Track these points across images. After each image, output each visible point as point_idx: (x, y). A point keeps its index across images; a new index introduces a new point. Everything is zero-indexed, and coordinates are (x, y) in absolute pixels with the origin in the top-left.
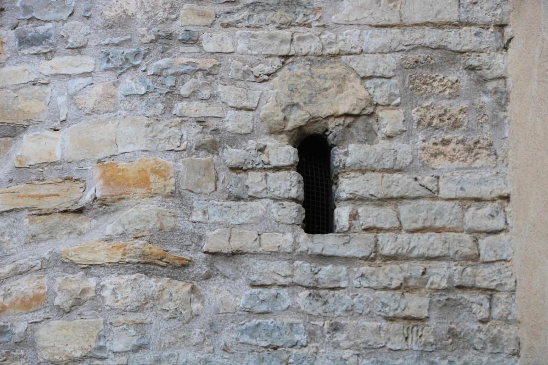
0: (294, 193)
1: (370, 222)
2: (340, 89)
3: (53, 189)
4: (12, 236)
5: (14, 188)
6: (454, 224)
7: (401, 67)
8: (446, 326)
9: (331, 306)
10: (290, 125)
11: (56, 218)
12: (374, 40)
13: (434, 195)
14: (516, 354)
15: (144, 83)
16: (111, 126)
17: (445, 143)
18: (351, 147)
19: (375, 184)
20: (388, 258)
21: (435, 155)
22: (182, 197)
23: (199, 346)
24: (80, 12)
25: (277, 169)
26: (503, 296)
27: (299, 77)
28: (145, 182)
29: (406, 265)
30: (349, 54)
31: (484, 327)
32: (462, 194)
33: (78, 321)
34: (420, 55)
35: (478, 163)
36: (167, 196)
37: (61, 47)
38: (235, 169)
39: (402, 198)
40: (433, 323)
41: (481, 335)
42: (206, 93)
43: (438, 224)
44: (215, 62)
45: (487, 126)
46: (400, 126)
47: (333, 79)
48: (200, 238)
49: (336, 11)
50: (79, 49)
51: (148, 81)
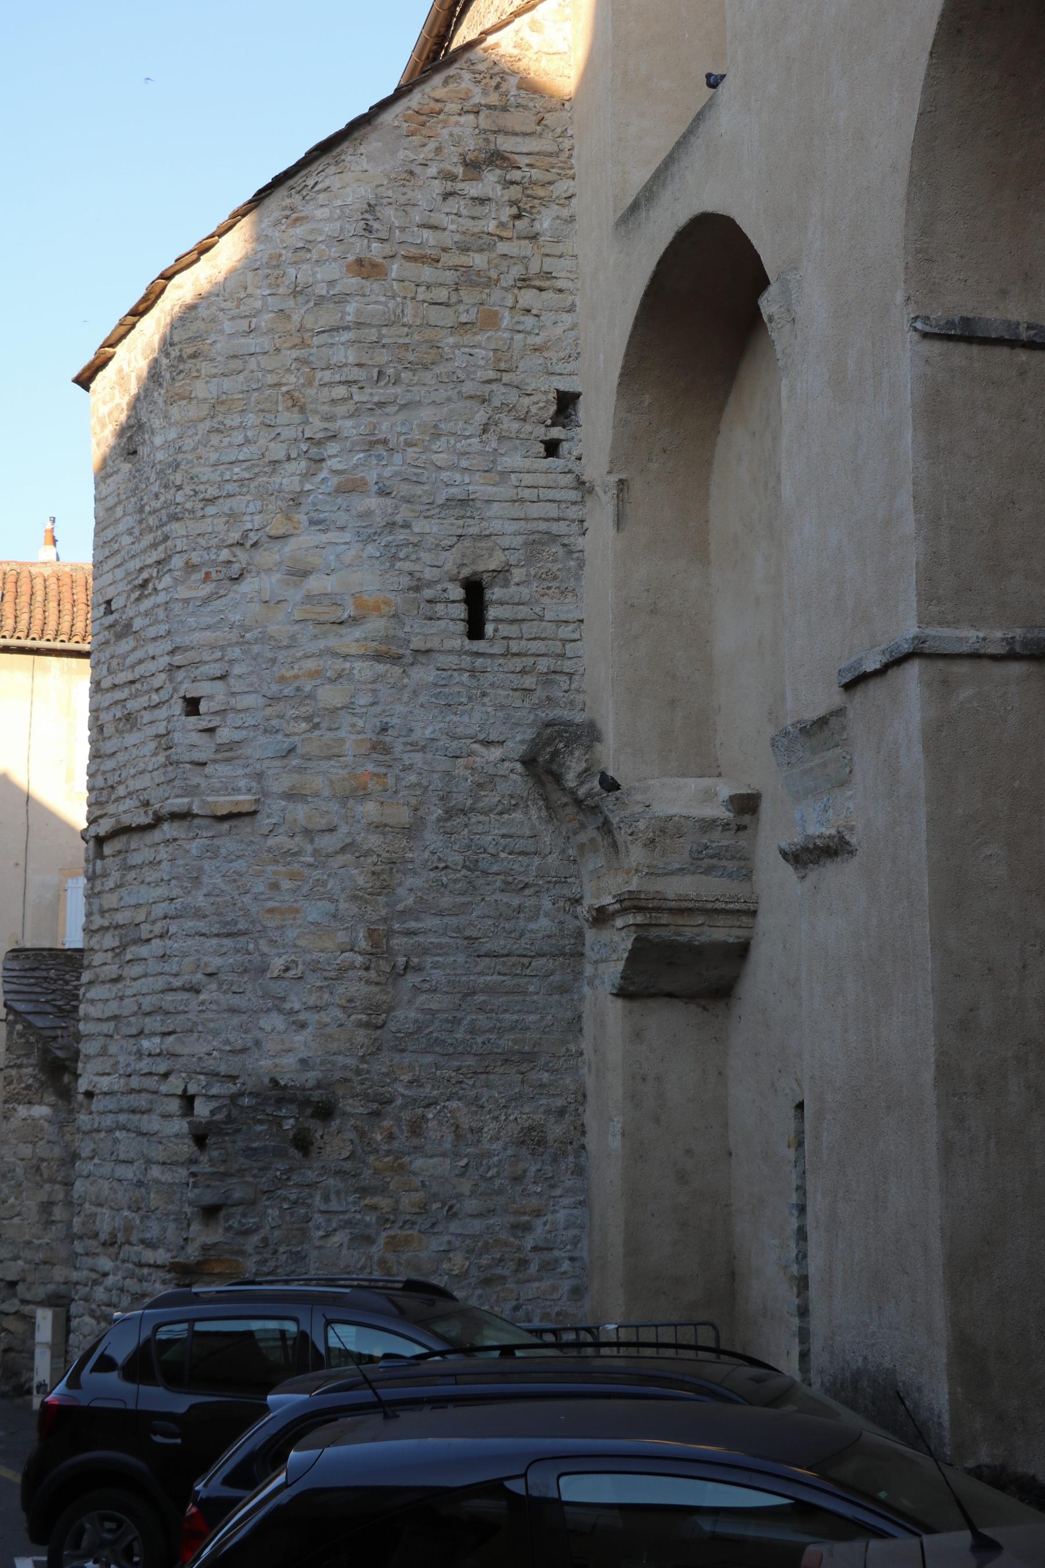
0: (462, 616)
1: (505, 634)
2: (490, 555)
3: (326, 609)
5: (304, 607)
6: (552, 636)
7: (525, 544)
8: (546, 694)
10: (461, 576)
11: (328, 626)
13: (541, 619)
14: (583, 710)
17: (549, 588)
18: (496, 590)
19: (518, 738)
20: (514, 655)
21: (543, 596)
23: (407, 704)
24: (344, 506)
25: (453, 602)
26: (577, 677)
28: (378, 609)
29: (524, 659)
31: (566, 695)
32: (557, 618)
34: (536, 537)
35: (567, 601)
37: (332, 527)
38: (429, 601)
40: (538, 692)
42: (414, 557)
43: (543, 636)
46: (524, 578)
48: (409, 641)
50: (342, 529)
51: (381, 549)
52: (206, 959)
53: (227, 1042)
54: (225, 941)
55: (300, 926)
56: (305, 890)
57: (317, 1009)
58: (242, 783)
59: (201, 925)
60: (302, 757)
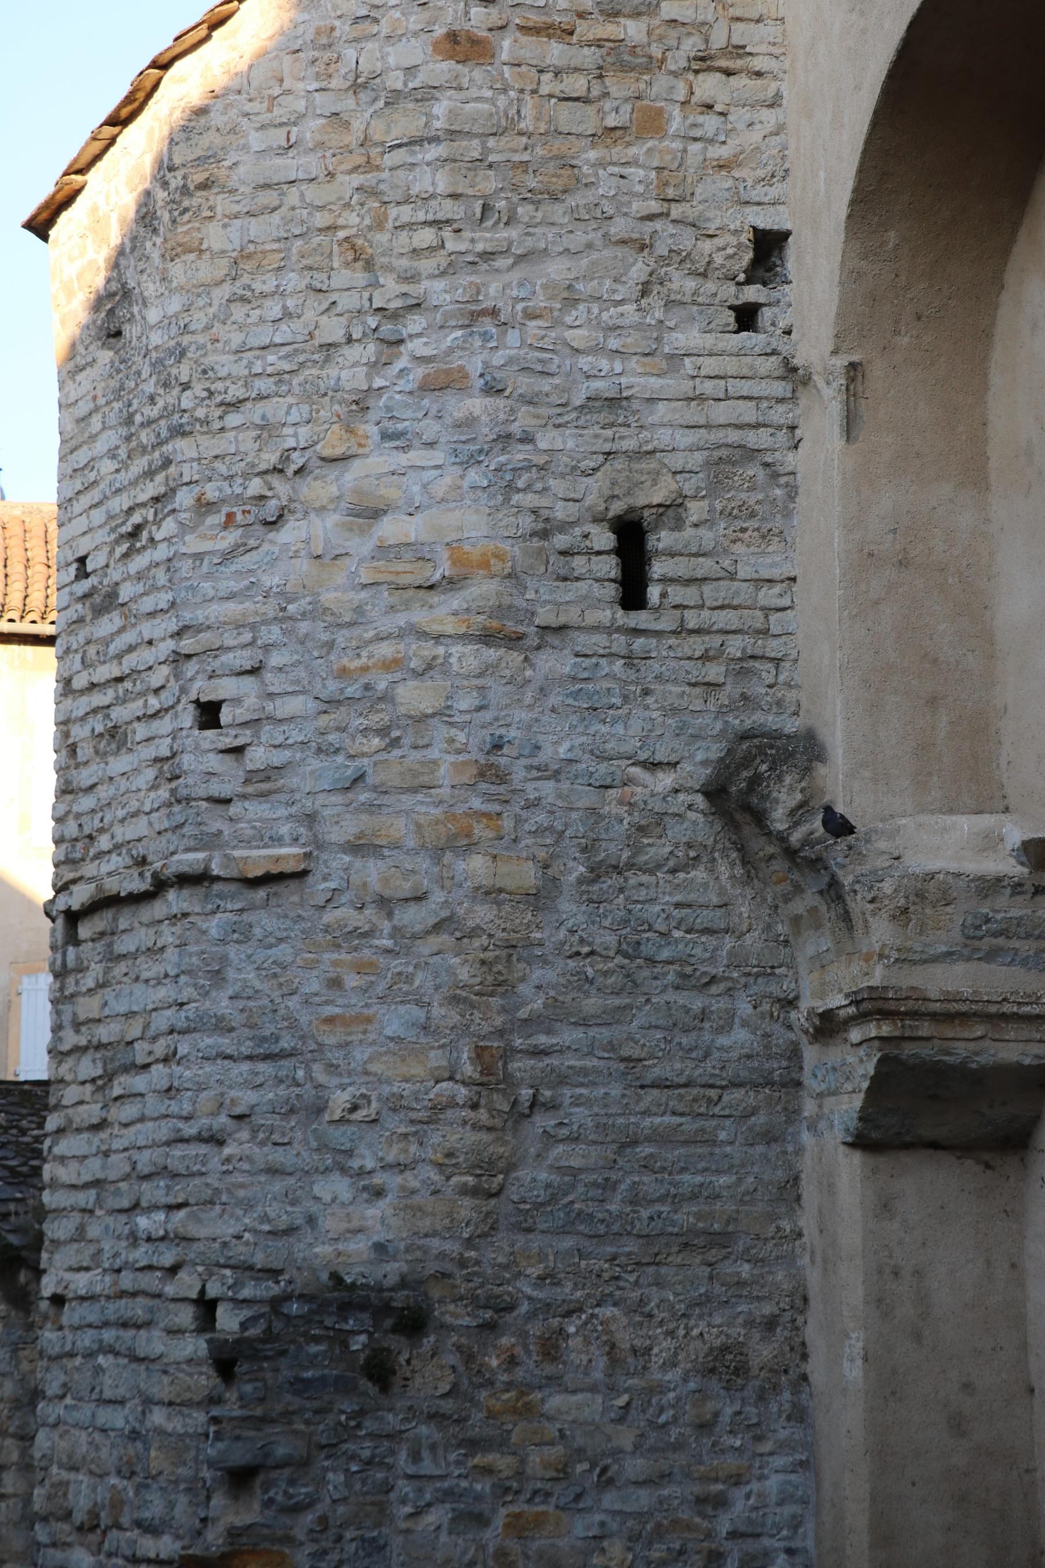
1: (678, 600)
2: (655, 483)
3: (408, 567)
4: (374, 606)
5: (375, 564)
6: (749, 602)
7: (707, 463)
8: (740, 691)
9: (642, 674)
10: (611, 514)
11: (411, 592)
12: (685, 439)
13: (732, 576)
14: (796, 714)
15: (486, 477)
16: (458, 513)
17: (743, 530)
18: (663, 534)
21: (734, 542)
22: (517, 578)
24: (433, 412)
25: (599, 553)
26: (787, 665)
27: (619, 471)
28: (485, 564)
29: (707, 638)
30: (663, 451)
32: (756, 576)
33: (429, 683)
34: (724, 452)
35: (770, 549)
36: (505, 577)
37: (416, 443)
38: (563, 553)
39: (705, 579)
40: (728, 688)
41: (768, 698)
42: (539, 486)
44: (547, 458)
45: (778, 516)
46: (705, 516)
47: (649, 473)
48: (533, 614)
49: (651, 413)
50: (431, 445)
51: (490, 475)
52: (233, 1094)
53: (265, 1218)
54: (262, 1067)
55: (374, 1043)
56: (381, 988)
57: (401, 1167)
58: (284, 830)
59: (225, 1043)
60: (375, 789)
